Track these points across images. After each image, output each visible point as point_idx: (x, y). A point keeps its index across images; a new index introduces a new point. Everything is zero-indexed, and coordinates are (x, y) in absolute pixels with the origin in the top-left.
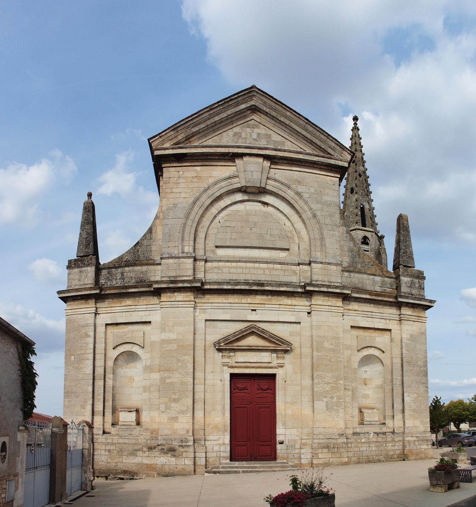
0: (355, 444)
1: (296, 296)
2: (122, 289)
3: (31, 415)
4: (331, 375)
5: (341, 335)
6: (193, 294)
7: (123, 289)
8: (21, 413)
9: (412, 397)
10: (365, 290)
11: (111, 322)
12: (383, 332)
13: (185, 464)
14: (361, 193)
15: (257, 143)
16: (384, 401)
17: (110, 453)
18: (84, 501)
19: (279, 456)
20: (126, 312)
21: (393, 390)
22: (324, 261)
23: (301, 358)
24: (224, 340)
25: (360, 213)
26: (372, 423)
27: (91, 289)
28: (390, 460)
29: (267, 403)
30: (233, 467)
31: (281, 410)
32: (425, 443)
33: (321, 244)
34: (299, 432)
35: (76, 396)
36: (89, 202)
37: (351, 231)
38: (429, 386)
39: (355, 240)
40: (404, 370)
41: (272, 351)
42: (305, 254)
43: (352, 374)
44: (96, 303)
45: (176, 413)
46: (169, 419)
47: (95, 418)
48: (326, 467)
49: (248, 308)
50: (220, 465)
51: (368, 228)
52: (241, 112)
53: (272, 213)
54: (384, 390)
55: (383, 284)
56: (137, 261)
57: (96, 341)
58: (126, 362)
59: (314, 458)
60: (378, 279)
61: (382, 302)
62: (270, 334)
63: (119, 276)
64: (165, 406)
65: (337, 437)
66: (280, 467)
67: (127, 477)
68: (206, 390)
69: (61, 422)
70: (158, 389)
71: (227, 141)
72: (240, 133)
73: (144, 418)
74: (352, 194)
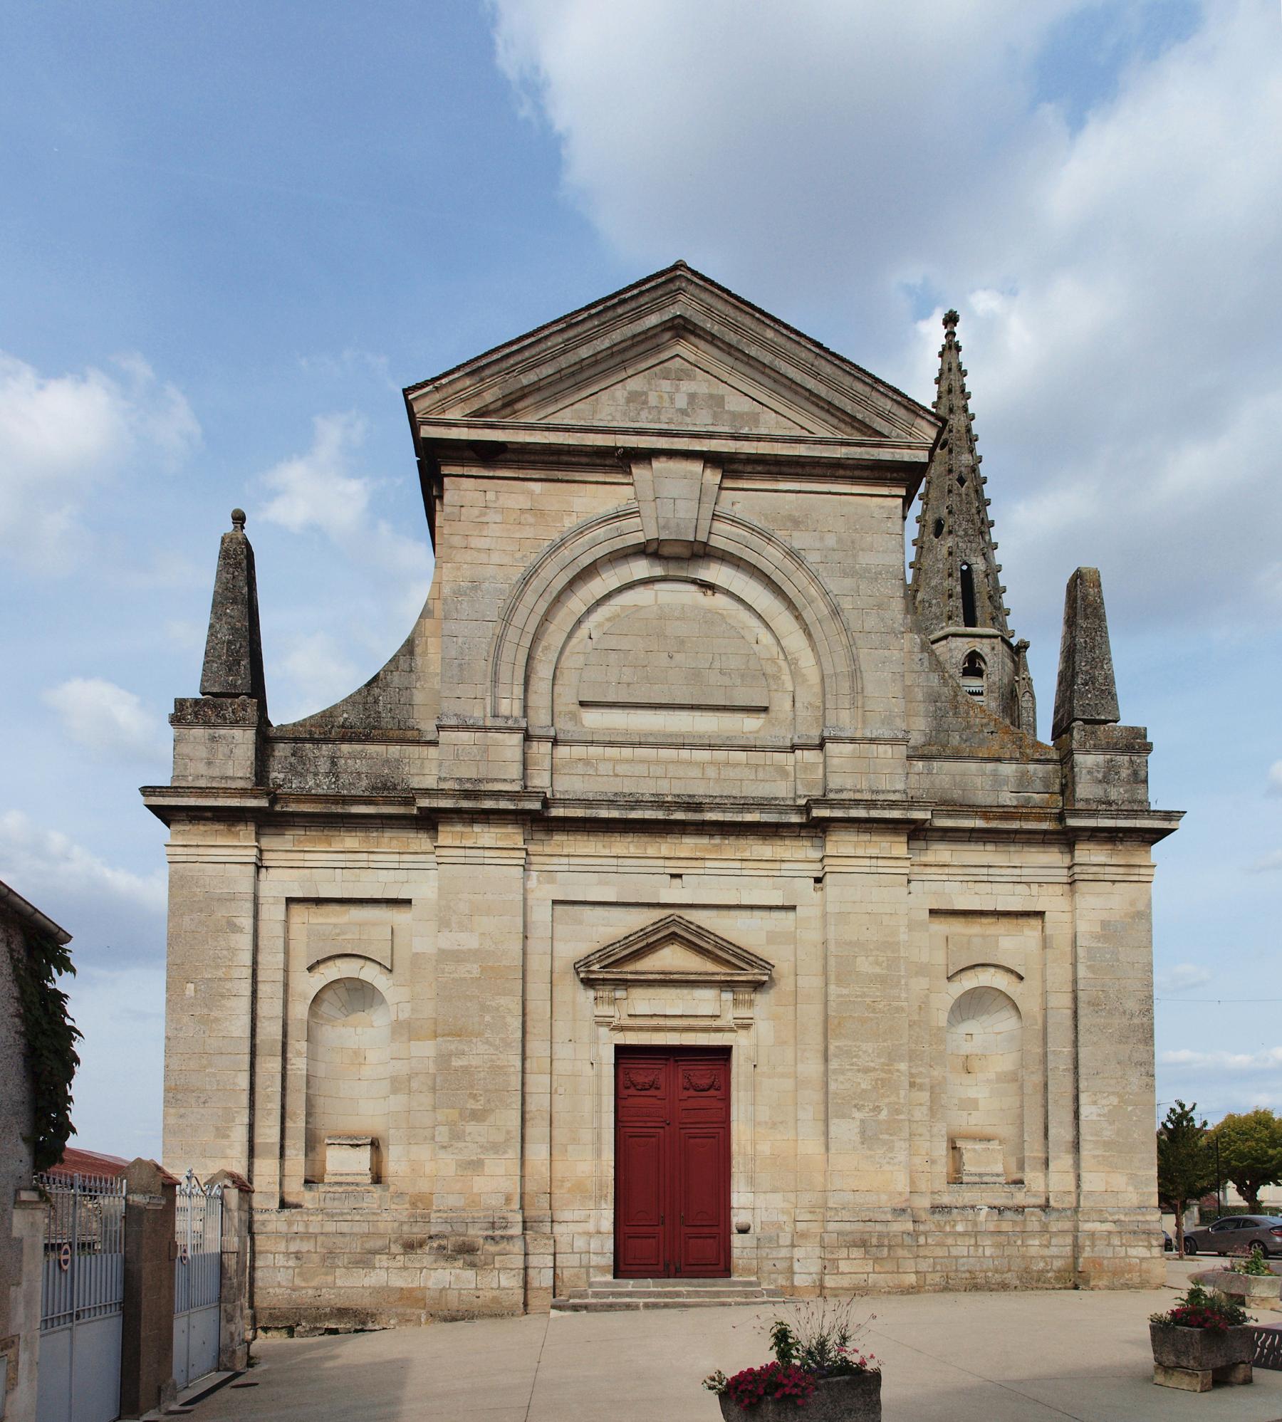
0: (937, 1236)
1: (785, 834)
2: (332, 803)
3: (61, 1155)
5: (903, 937)
6: (520, 831)
7: (336, 802)
8: (23, 1151)
10: (970, 806)
11: (300, 895)
12: (1021, 921)
13: (499, 1286)
14: (964, 530)
15: (688, 420)
17: (299, 1263)
18: (228, 1401)
20: (344, 870)
21: (1046, 1085)
22: (858, 735)
23: (796, 1004)
24: (600, 956)
25: (959, 589)
26: (986, 1179)
27: (243, 793)
28: (1035, 1285)
30: (620, 1295)
31: (743, 1142)
32: (1142, 1240)
33: (852, 688)
34: (788, 1201)
35: (202, 1100)
36: (237, 538)
37: (934, 642)
38: (1157, 1071)
39: (944, 668)
40: (1080, 1027)
42: (809, 718)
43: (932, 1045)
44: (258, 836)
45: (479, 1150)
46: (460, 1166)
47: (258, 1163)
48: (858, 1298)
49: (661, 870)
50: (589, 1288)
51: (982, 627)
52: (648, 335)
53: (725, 612)
54: (1021, 1087)
55: (1023, 783)
56: (375, 728)
57: (260, 943)
58: (343, 1009)
59: (826, 1272)
60: (1008, 769)
61: (1018, 836)
63: (324, 766)
64: (450, 1130)
65: (889, 1217)
66: (739, 1294)
67: (348, 1326)
68: (556, 1088)
69: (155, 1176)
70: (430, 1083)
71: (611, 414)
72: (645, 394)
73: (394, 1163)
74: (937, 537)
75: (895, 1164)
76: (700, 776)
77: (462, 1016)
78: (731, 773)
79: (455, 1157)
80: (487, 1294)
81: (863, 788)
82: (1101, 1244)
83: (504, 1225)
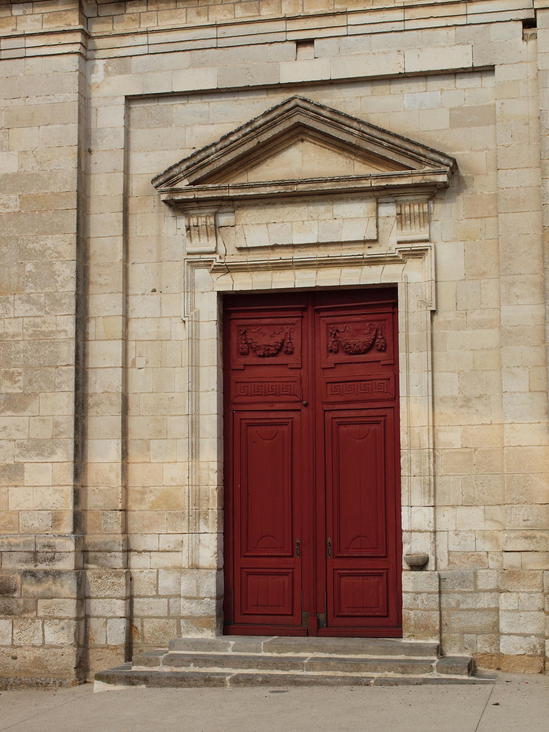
13: (44, 643)
24: (188, 168)
29: (367, 405)
31: (417, 430)
34: (492, 520)
41: (377, 194)
45: (17, 451)
49: (282, 37)
62: (363, 128)
68: (134, 361)
80: (27, 653)
83: (50, 555)
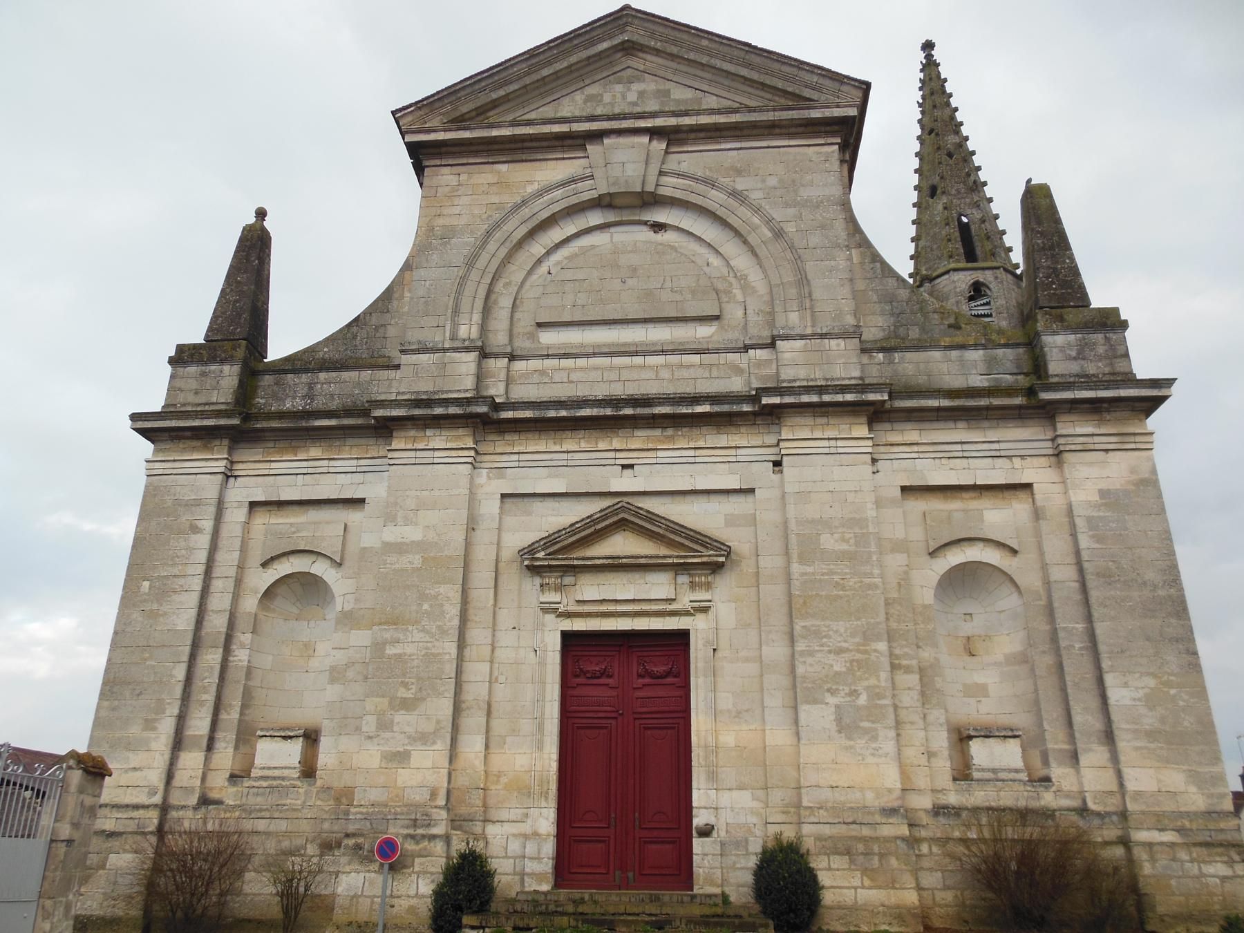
4: (848, 626)
9: (1137, 688)
16: (1037, 703)
19: (699, 874)
20: (305, 476)
24: (545, 544)
26: (1002, 775)
34: (757, 800)
35: (138, 692)
42: (761, 322)
44: (231, 450)
45: (406, 741)
46: (385, 758)
49: (612, 462)
53: (676, 244)
54: (1032, 670)
60: (976, 355)
62: (668, 524)
63: (303, 391)
64: (378, 719)
65: (878, 818)
68: (497, 679)
72: (601, 95)
73: (326, 757)
74: (932, 198)
75: (880, 756)
76: (654, 377)
77: (400, 605)
78: (685, 373)
79: (381, 748)
81: (817, 377)
82: (1162, 862)
